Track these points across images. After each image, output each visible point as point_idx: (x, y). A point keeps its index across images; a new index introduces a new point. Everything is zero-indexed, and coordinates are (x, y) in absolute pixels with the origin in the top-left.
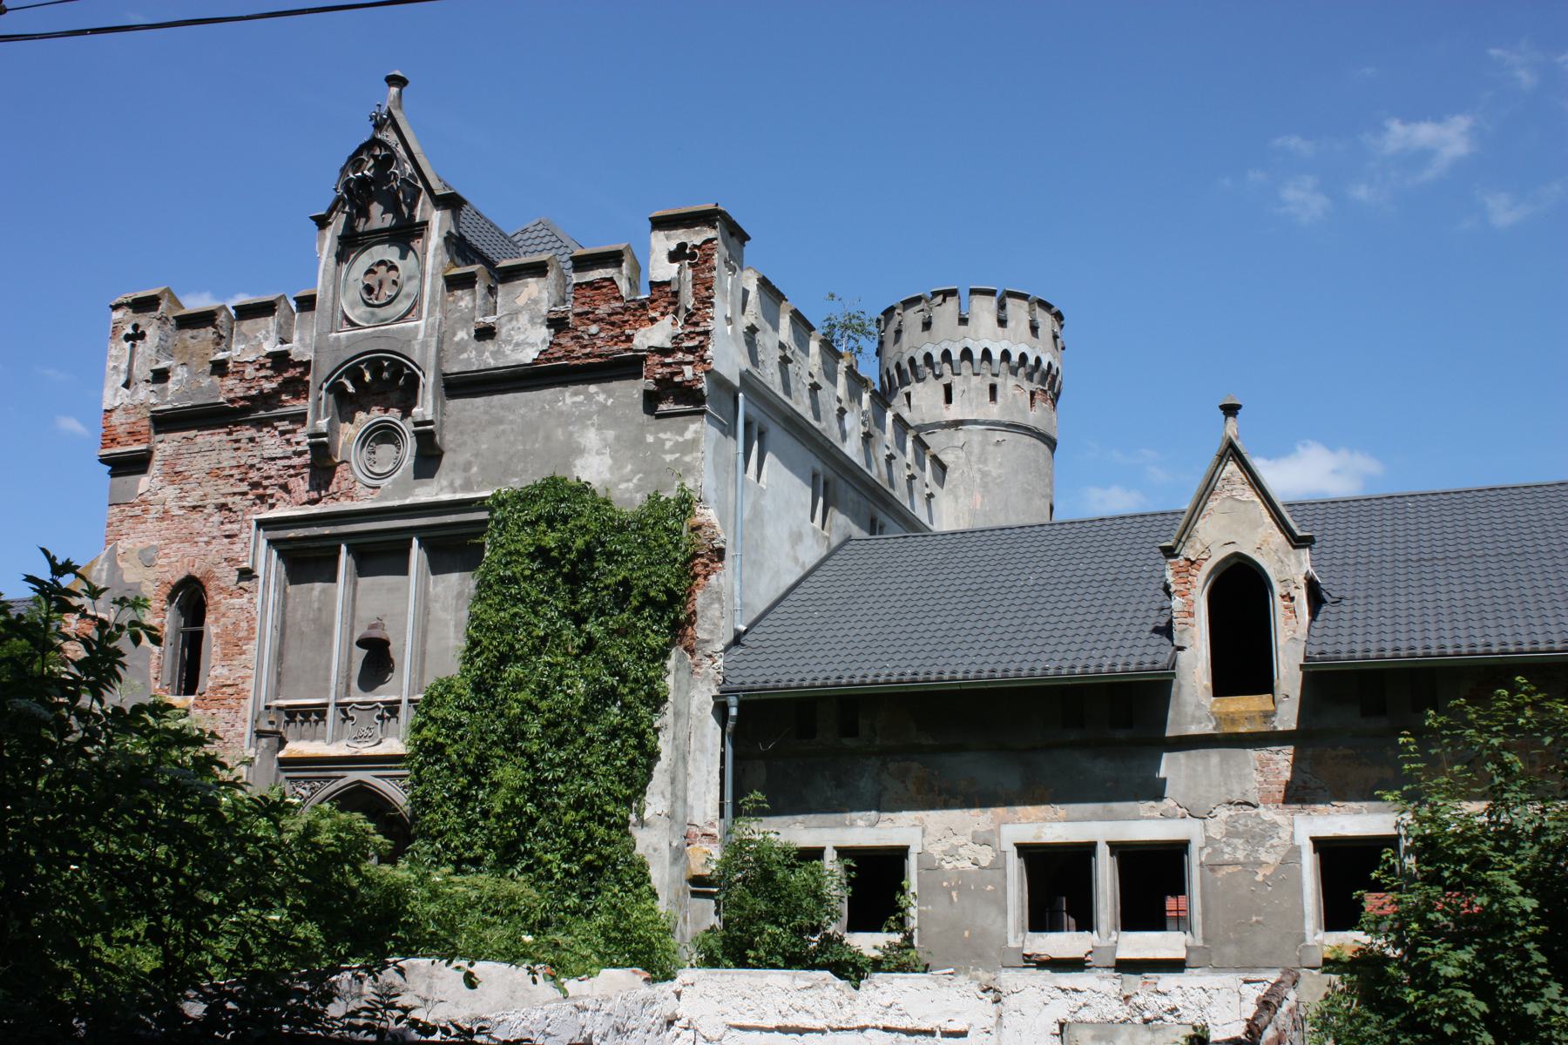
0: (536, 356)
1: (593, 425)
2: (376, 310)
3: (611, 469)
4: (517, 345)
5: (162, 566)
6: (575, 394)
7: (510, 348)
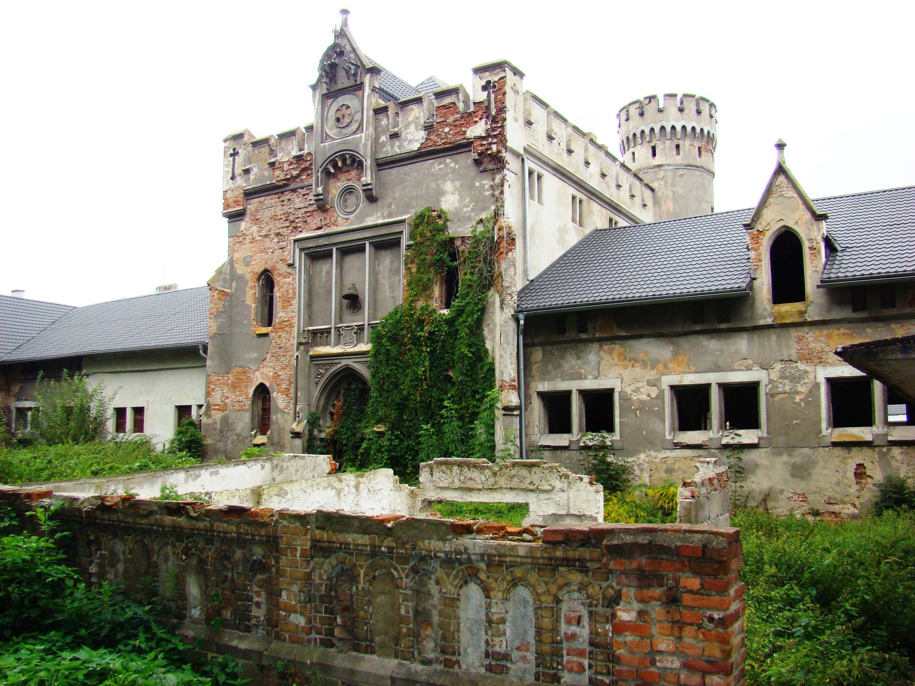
2: (343, 130)
3: (459, 202)
4: (410, 141)
6: (440, 164)
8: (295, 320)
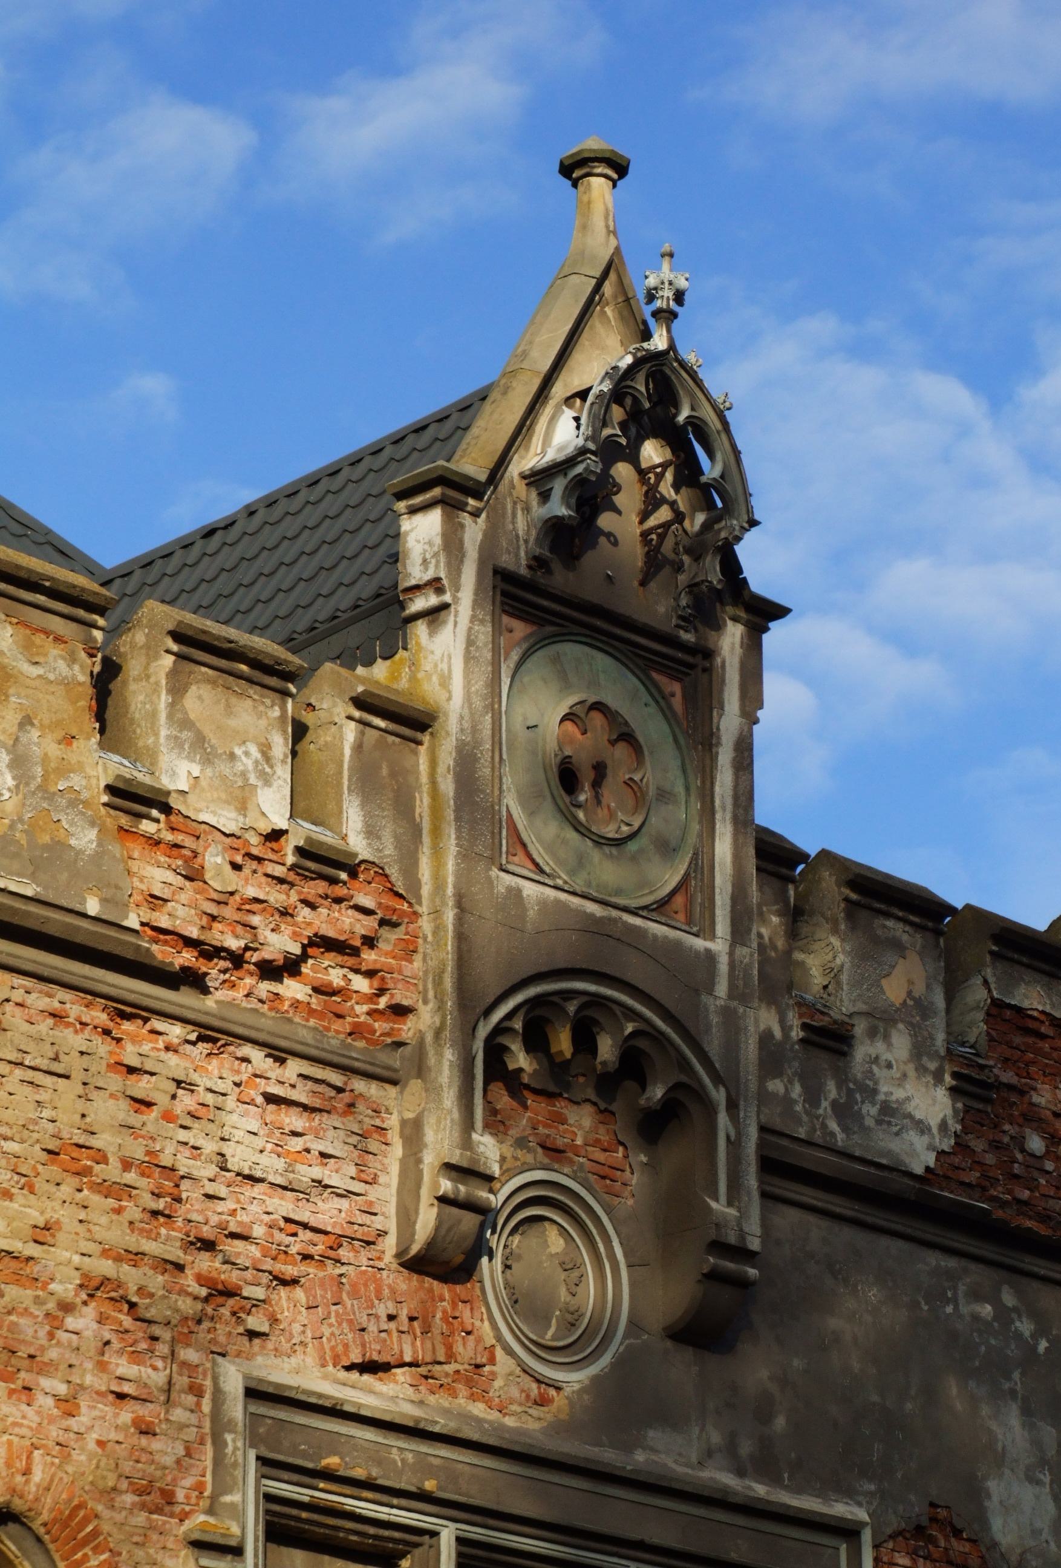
1: (1013, 1393)
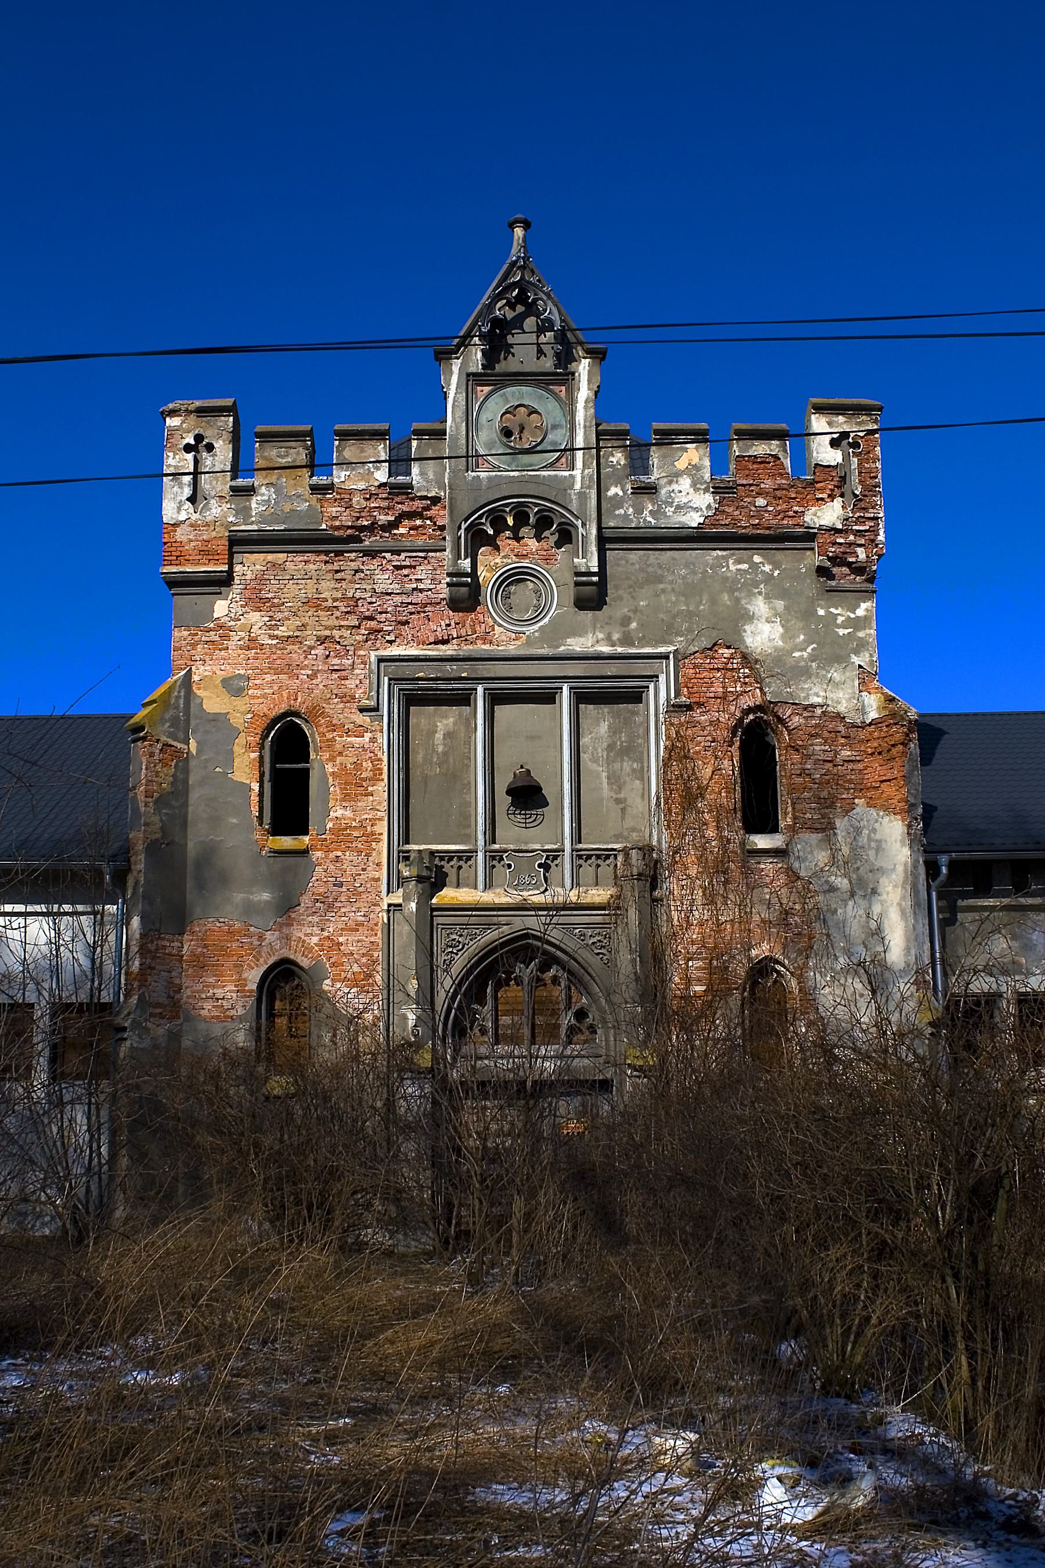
0: (701, 520)
1: (760, 593)
3: (783, 637)
4: (679, 507)
5: (253, 697)
6: (739, 562)
7: (672, 509)
8: (382, 828)
